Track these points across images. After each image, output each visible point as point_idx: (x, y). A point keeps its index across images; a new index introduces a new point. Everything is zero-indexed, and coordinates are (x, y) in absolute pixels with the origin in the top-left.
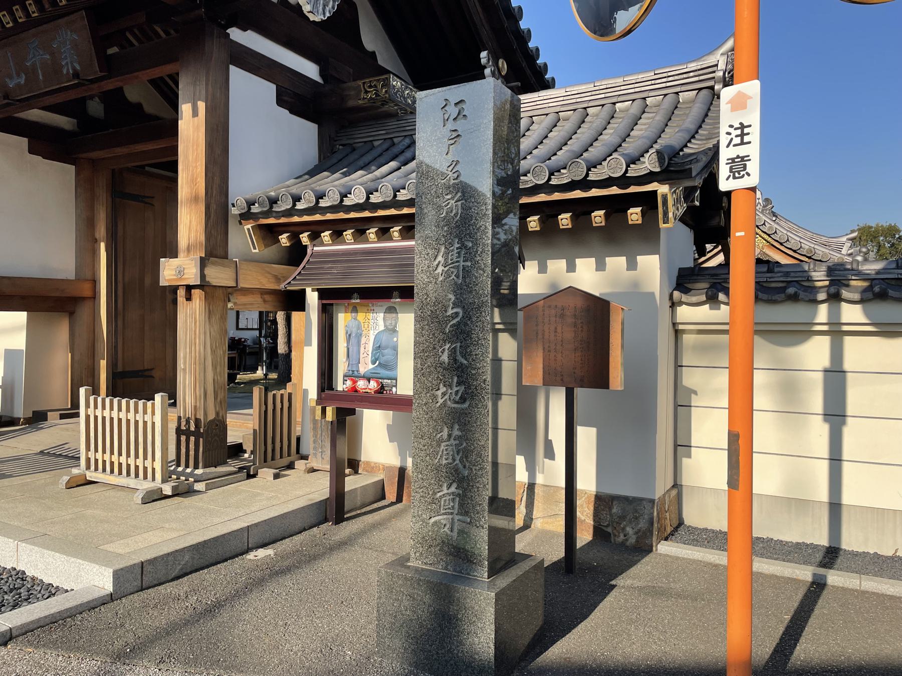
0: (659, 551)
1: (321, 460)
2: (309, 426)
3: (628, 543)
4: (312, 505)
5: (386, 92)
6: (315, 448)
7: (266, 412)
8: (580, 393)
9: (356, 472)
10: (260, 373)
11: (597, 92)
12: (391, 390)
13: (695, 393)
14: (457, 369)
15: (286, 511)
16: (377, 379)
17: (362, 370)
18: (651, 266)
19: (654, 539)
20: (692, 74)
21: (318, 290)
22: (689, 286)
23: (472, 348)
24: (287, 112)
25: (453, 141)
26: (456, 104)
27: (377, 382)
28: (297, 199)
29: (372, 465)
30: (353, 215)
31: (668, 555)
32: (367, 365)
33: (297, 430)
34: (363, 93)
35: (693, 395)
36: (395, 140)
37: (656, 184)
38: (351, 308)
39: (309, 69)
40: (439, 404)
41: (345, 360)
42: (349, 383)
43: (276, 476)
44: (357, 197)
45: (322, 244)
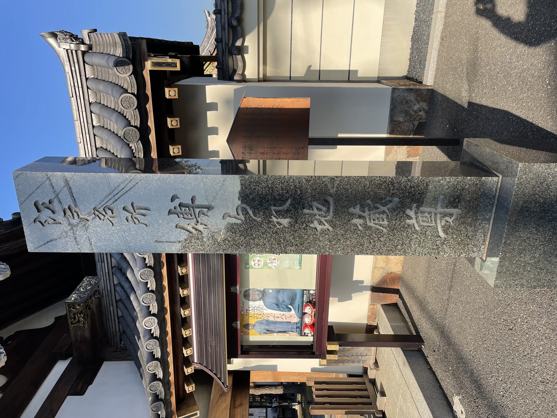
0: (432, 84)
1: (367, 355)
2: (340, 367)
3: (426, 108)
4: (409, 363)
5: (79, 305)
6: (359, 362)
7: (331, 403)
8: (313, 134)
9: (376, 327)
10: (297, 407)
11: (85, 140)
12: (312, 295)
13: (310, 67)
14: (296, 209)
15: (416, 385)
16: (303, 307)
17: (296, 319)
18: (214, 92)
19: (422, 88)
20: (73, 69)
21: (229, 358)
22: (231, 71)
23: (276, 194)
24: (90, 387)
25: (75, 214)
26: (39, 211)
27: (306, 306)
28: (154, 377)
29: (370, 314)
30: (169, 329)
31: (435, 77)
32: (293, 316)
33: (343, 377)
34: (81, 327)
35: (312, 69)
36: (118, 298)
37: (144, 72)
38: (245, 330)
39: (60, 367)
40: (330, 228)
41: (288, 335)
42: (307, 331)
43: (383, 394)
44: (153, 324)
45: (192, 356)
